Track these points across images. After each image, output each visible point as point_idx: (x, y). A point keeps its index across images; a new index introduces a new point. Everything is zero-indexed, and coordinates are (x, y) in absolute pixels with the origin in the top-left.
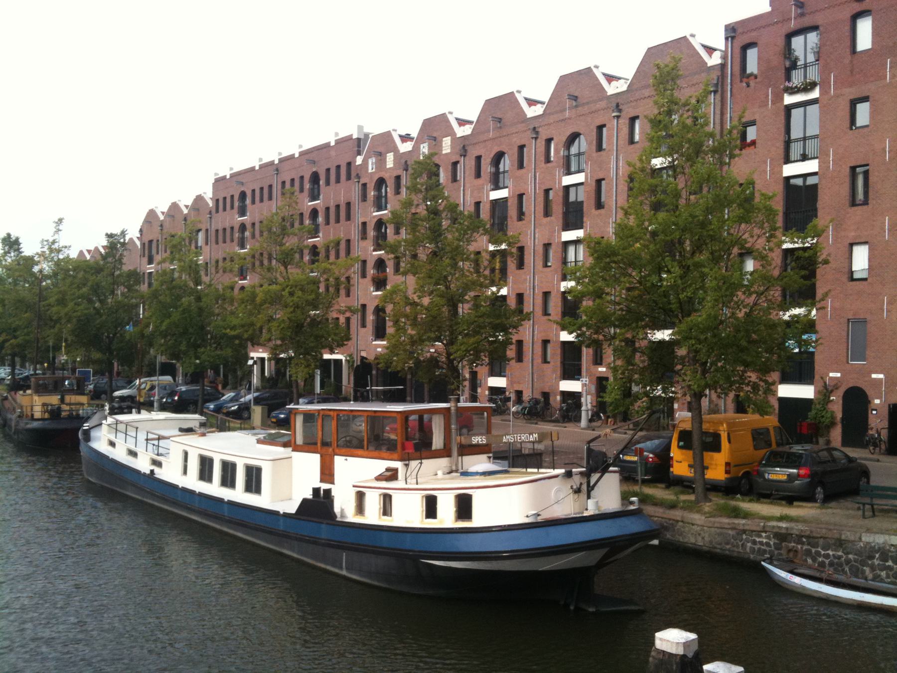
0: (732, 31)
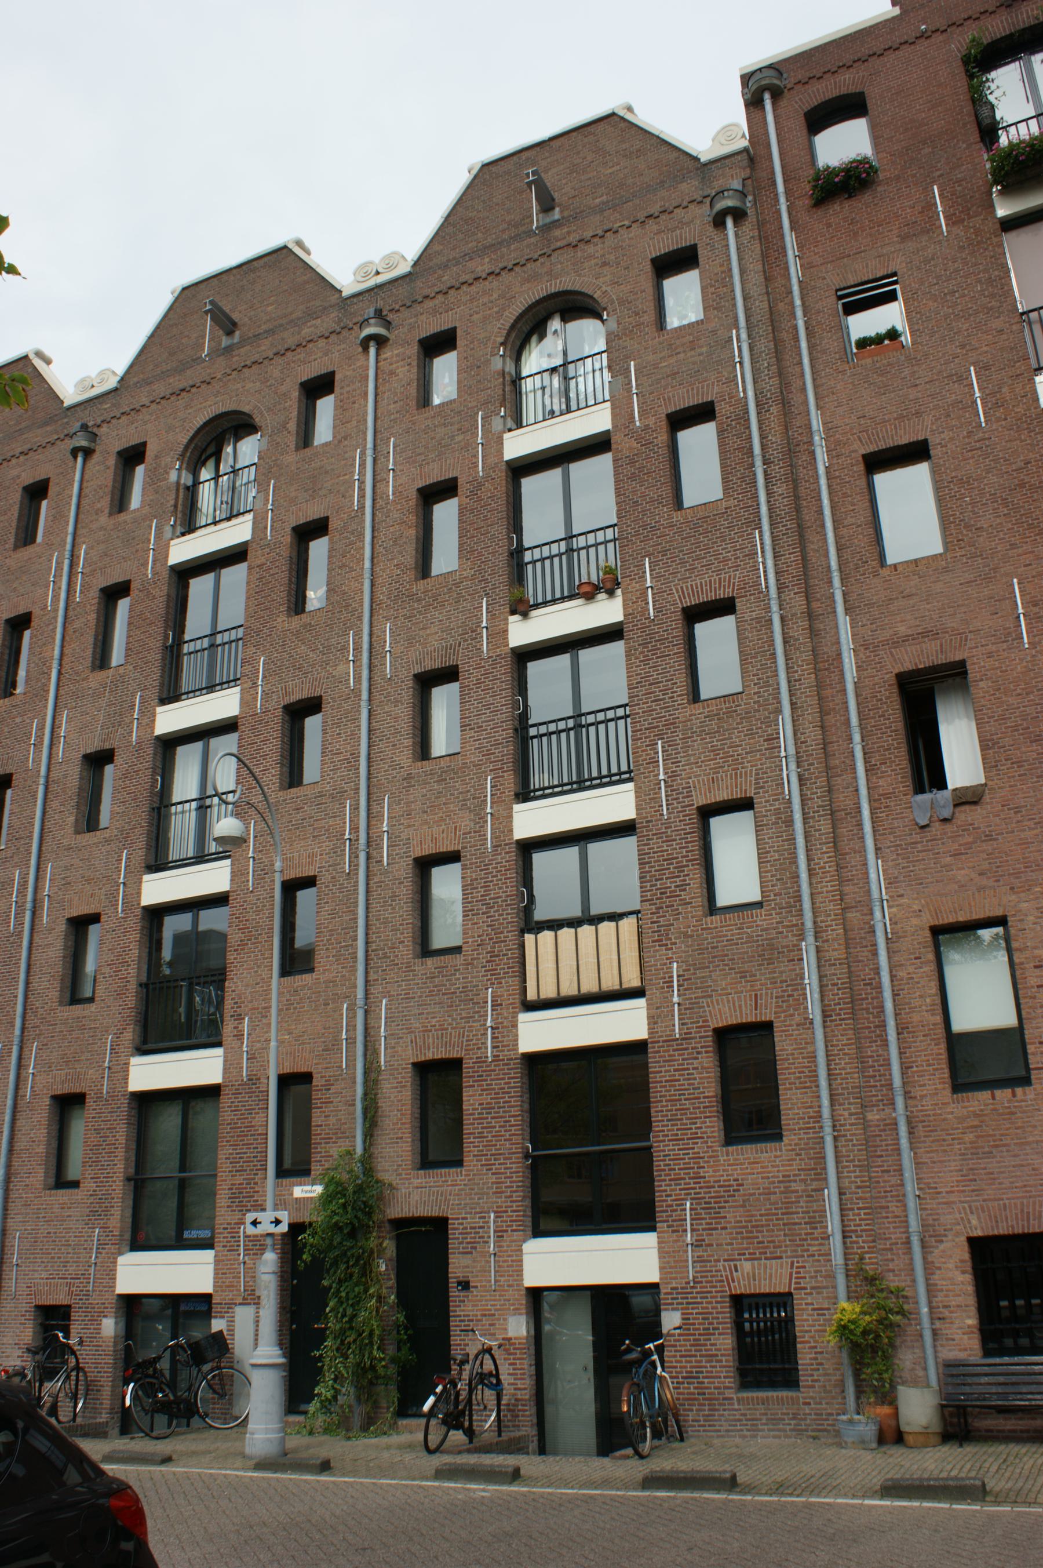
0: (762, 88)
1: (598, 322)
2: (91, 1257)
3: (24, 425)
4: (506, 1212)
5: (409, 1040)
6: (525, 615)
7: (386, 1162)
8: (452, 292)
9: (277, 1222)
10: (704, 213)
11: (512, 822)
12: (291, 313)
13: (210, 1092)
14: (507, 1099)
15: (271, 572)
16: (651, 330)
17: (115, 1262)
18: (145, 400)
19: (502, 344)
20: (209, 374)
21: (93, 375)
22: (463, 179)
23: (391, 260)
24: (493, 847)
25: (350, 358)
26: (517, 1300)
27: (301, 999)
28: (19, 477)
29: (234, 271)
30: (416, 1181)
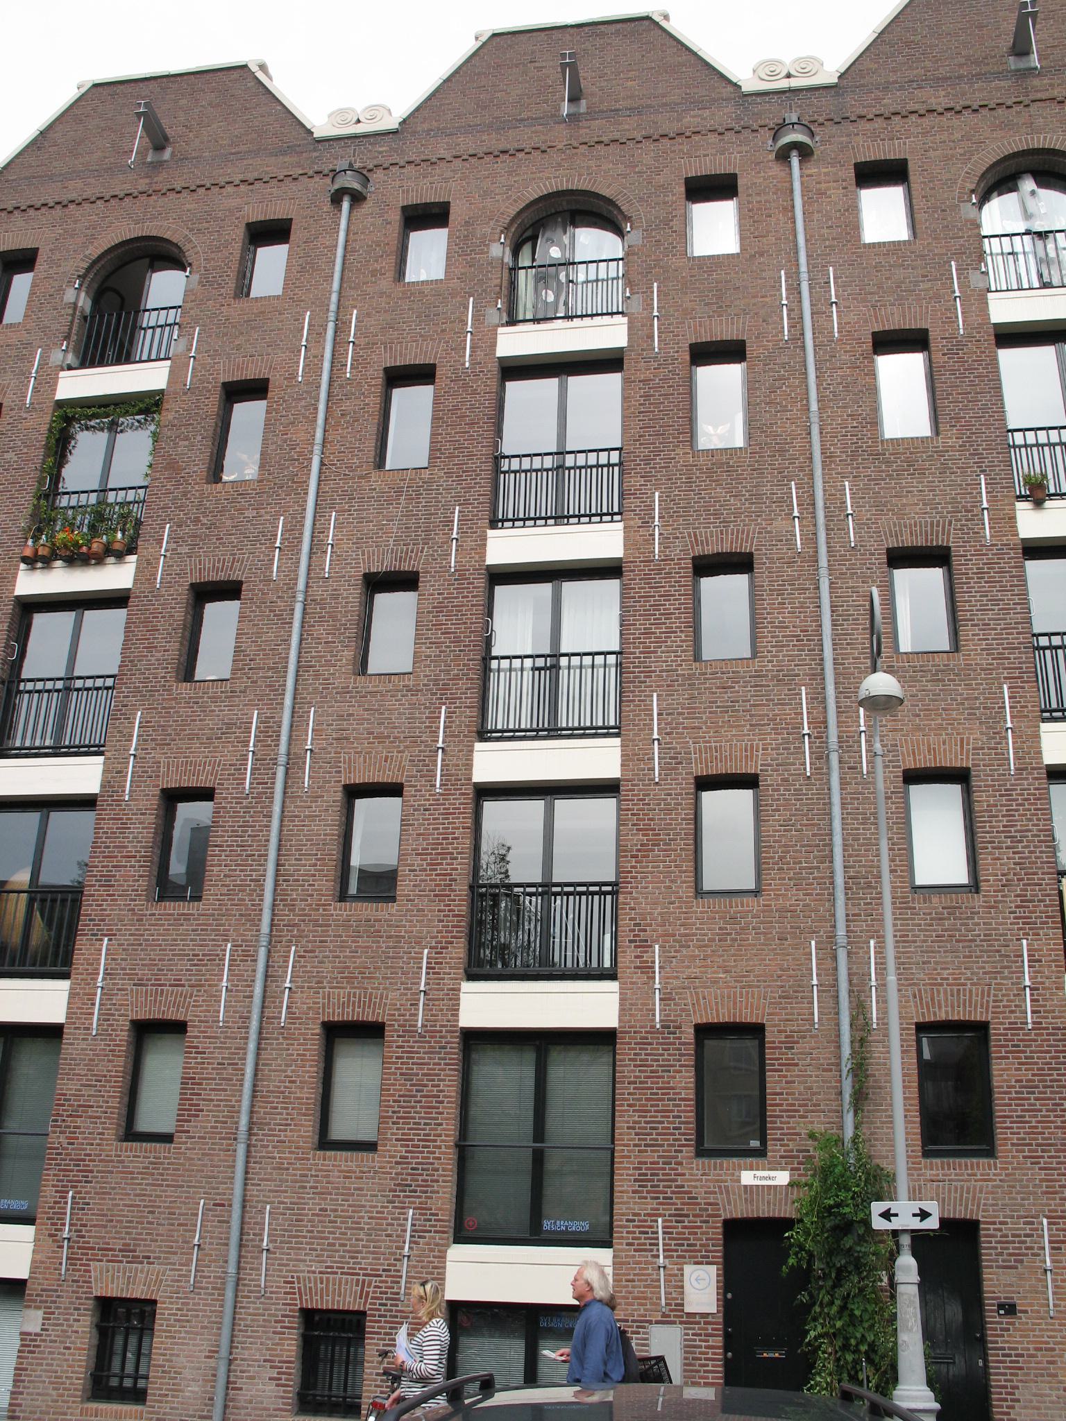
1: (619, 240)
2: (403, 1248)
3: (243, 148)
6: (1038, 504)
7: (883, 1146)
8: (897, 119)
9: (924, 1215)
11: (1039, 742)
13: (50, 1033)
16: (385, 283)
17: (443, 1257)
18: (442, 153)
19: (973, 191)
21: (787, 60)
22: (464, 47)
23: (808, 64)
24: (1016, 769)
27: (741, 929)
29: (571, 31)
30: (928, 1172)
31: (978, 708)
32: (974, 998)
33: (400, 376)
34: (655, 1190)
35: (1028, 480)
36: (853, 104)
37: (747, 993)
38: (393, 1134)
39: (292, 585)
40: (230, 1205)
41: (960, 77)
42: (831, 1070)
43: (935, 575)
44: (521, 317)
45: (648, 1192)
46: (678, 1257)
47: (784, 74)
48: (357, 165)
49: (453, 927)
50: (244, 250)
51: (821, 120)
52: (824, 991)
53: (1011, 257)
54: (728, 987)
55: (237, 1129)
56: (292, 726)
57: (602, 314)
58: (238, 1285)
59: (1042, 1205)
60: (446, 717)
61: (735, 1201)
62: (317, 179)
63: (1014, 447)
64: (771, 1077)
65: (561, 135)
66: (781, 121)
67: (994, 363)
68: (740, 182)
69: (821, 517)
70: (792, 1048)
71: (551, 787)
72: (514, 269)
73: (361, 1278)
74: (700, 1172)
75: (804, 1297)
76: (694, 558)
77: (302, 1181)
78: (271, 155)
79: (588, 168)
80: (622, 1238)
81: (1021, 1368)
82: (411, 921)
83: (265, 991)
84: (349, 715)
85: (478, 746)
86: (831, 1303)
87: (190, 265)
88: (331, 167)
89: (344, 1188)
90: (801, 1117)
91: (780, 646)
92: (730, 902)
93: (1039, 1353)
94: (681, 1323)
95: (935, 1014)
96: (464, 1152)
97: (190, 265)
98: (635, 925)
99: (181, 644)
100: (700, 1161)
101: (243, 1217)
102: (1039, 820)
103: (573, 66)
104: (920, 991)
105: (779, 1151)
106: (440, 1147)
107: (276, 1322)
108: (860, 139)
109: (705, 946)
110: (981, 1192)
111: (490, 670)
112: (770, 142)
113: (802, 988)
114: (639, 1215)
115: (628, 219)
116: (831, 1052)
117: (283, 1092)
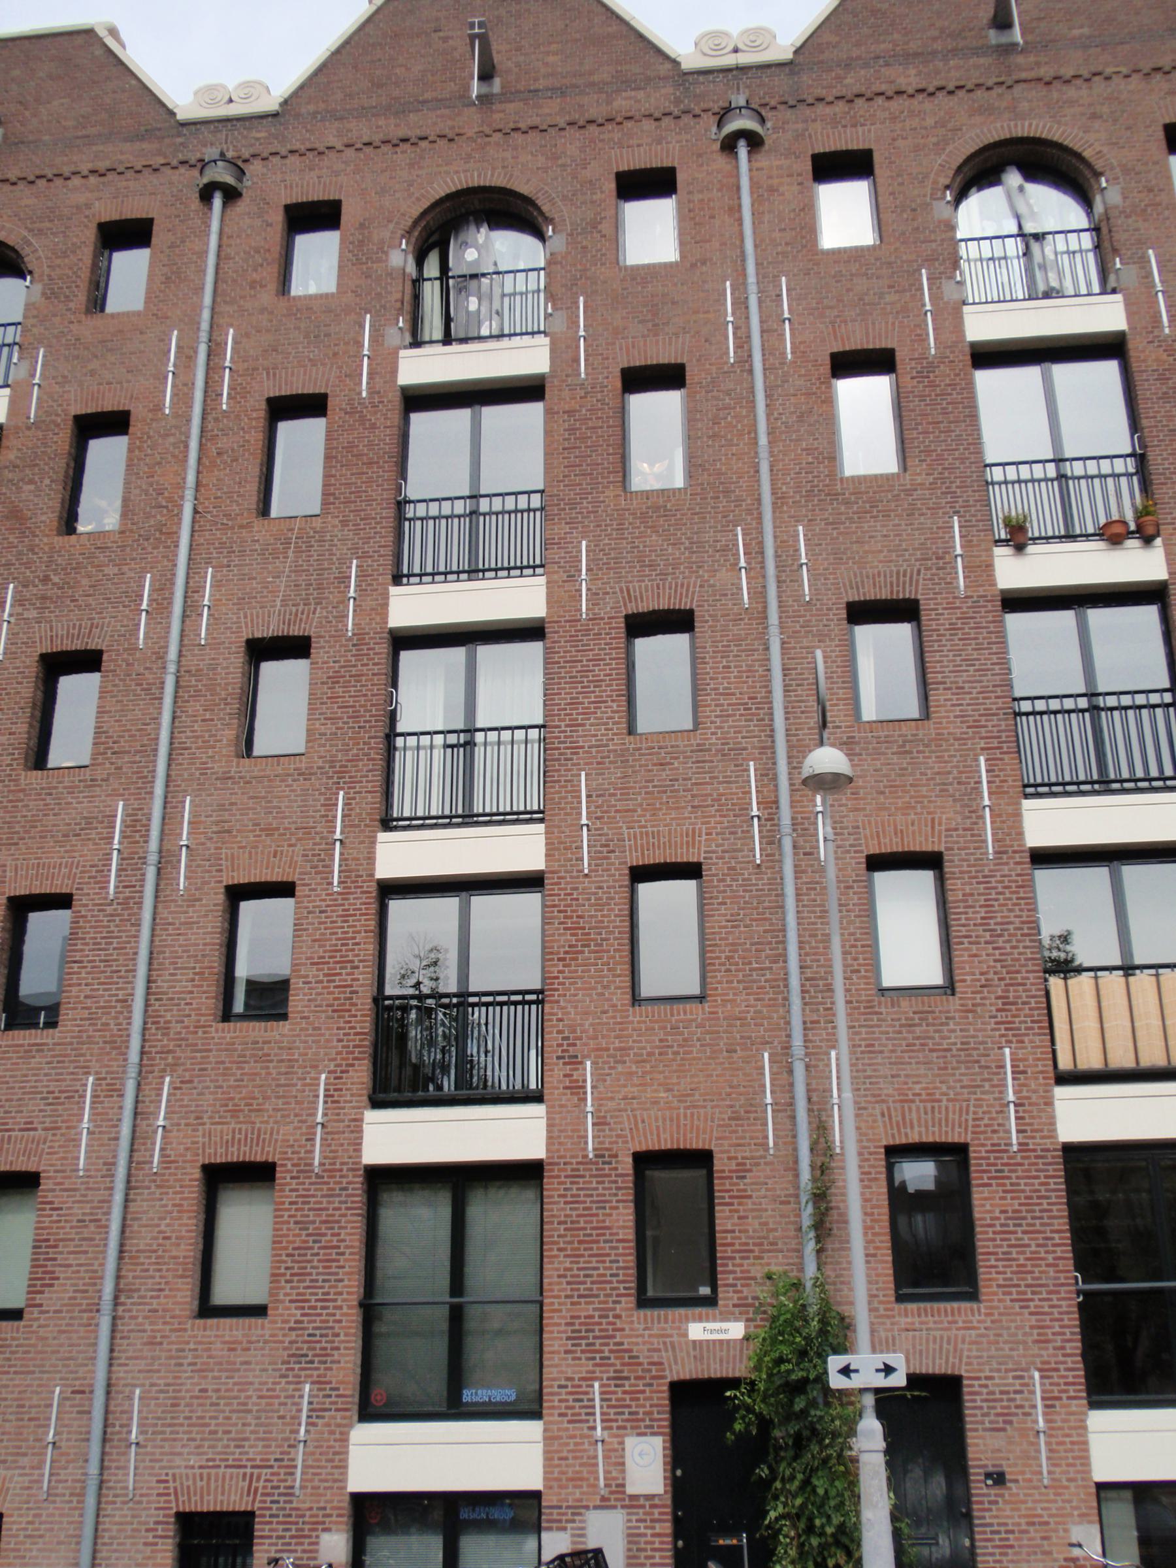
2: (297, 1432)
3: (92, 131)
4: (1057, 1370)
5: (878, 1112)
6: (1020, 548)
8: (860, 102)
9: (888, 1370)
10: (191, 181)
12: (591, 73)
14: (1045, 1206)
15: (590, 424)
16: (267, 296)
17: (344, 1440)
18: (332, 141)
19: (947, 187)
20: (452, 128)
24: (995, 853)
25: (700, 155)
26: (1085, 1501)
28: (88, 206)
30: (903, 1320)
31: (951, 784)
32: (951, 1115)
33: (286, 408)
34: (590, 1350)
35: (1007, 522)
36: (810, 83)
37: (692, 1114)
38: (286, 1294)
39: (161, 656)
40: (92, 1392)
41: (934, 53)
42: (789, 1203)
43: (903, 631)
44: (427, 338)
45: (583, 1352)
46: (619, 1428)
47: (730, 48)
48: (230, 154)
49: (355, 1047)
50: (97, 256)
51: (773, 103)
52: (778, 1111)
53: (1003, 262)
54: (671, 1108)
55: (100, 1298)
56: (164, 819)
57: (522, 334)
58: (100, 1488)
59: (1033, 1356)
60: (345, 804)
61: (683, 1359)
62: (182, 170)
63: (993, 483)
64: (721, 1212)
65: (470, 121)
66: (727, 105)
67: (970, 386)
68: (680, 177)
69: (772, 569)
70: (744, 1177)
71: (467, 870)
72: (418, 282)
73: (249, 1471)
74: (642, 1326)
75: (764, 1472)
76: (627, 617)
77: (179, 1357)
78: (126, 140)
79: (503, 159)
80: (553, 1407)
81: (1011, 1547)
82: (306, 1042)
83: (134, 1132)
84: (232, 804)
85: (382, 836)
86: (792, 1478)
87: (30, 273)
88: (198, 156)
89: (229, 1363)
90: (756, 1258)
91: (724, 717)
92: (672, 1010)
93: (1031, 1529)
94: (623, 1507)
95: (906, 1135)
96: (370, 1311)
97: (30, 273)
98: (564, 1039)
99: (31, 726)
100: (642, 1312)
101: (107, 1406)
102: (1021, 910)
103: (484, 39)
104: (889, 1109)
105: (732, 1298)
106: (341, 1308)
107: (147, 1530)
108: (818, 125)
109: (644, 1061)
110: (963, 1342)
111: (395, 749)
112: (714, 129)
113: (754, 1108)
114: (572, 1379)
115: (549, 221)
116: (790, 1182)
117: (155, 1251)
